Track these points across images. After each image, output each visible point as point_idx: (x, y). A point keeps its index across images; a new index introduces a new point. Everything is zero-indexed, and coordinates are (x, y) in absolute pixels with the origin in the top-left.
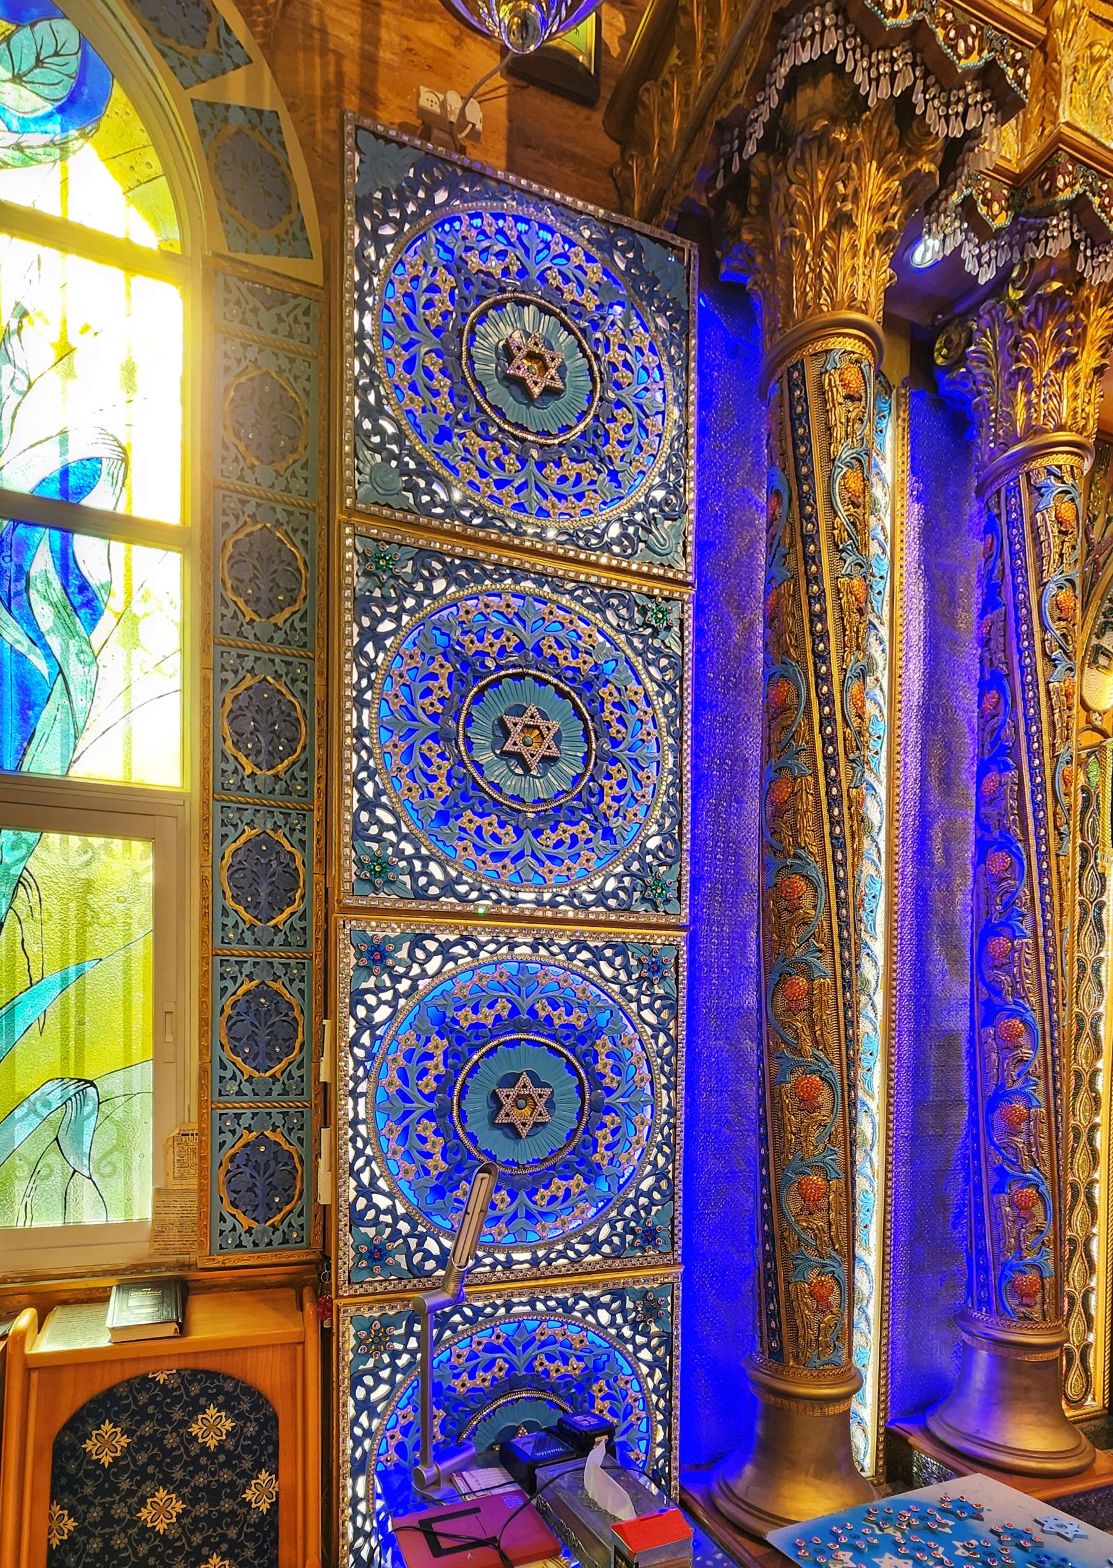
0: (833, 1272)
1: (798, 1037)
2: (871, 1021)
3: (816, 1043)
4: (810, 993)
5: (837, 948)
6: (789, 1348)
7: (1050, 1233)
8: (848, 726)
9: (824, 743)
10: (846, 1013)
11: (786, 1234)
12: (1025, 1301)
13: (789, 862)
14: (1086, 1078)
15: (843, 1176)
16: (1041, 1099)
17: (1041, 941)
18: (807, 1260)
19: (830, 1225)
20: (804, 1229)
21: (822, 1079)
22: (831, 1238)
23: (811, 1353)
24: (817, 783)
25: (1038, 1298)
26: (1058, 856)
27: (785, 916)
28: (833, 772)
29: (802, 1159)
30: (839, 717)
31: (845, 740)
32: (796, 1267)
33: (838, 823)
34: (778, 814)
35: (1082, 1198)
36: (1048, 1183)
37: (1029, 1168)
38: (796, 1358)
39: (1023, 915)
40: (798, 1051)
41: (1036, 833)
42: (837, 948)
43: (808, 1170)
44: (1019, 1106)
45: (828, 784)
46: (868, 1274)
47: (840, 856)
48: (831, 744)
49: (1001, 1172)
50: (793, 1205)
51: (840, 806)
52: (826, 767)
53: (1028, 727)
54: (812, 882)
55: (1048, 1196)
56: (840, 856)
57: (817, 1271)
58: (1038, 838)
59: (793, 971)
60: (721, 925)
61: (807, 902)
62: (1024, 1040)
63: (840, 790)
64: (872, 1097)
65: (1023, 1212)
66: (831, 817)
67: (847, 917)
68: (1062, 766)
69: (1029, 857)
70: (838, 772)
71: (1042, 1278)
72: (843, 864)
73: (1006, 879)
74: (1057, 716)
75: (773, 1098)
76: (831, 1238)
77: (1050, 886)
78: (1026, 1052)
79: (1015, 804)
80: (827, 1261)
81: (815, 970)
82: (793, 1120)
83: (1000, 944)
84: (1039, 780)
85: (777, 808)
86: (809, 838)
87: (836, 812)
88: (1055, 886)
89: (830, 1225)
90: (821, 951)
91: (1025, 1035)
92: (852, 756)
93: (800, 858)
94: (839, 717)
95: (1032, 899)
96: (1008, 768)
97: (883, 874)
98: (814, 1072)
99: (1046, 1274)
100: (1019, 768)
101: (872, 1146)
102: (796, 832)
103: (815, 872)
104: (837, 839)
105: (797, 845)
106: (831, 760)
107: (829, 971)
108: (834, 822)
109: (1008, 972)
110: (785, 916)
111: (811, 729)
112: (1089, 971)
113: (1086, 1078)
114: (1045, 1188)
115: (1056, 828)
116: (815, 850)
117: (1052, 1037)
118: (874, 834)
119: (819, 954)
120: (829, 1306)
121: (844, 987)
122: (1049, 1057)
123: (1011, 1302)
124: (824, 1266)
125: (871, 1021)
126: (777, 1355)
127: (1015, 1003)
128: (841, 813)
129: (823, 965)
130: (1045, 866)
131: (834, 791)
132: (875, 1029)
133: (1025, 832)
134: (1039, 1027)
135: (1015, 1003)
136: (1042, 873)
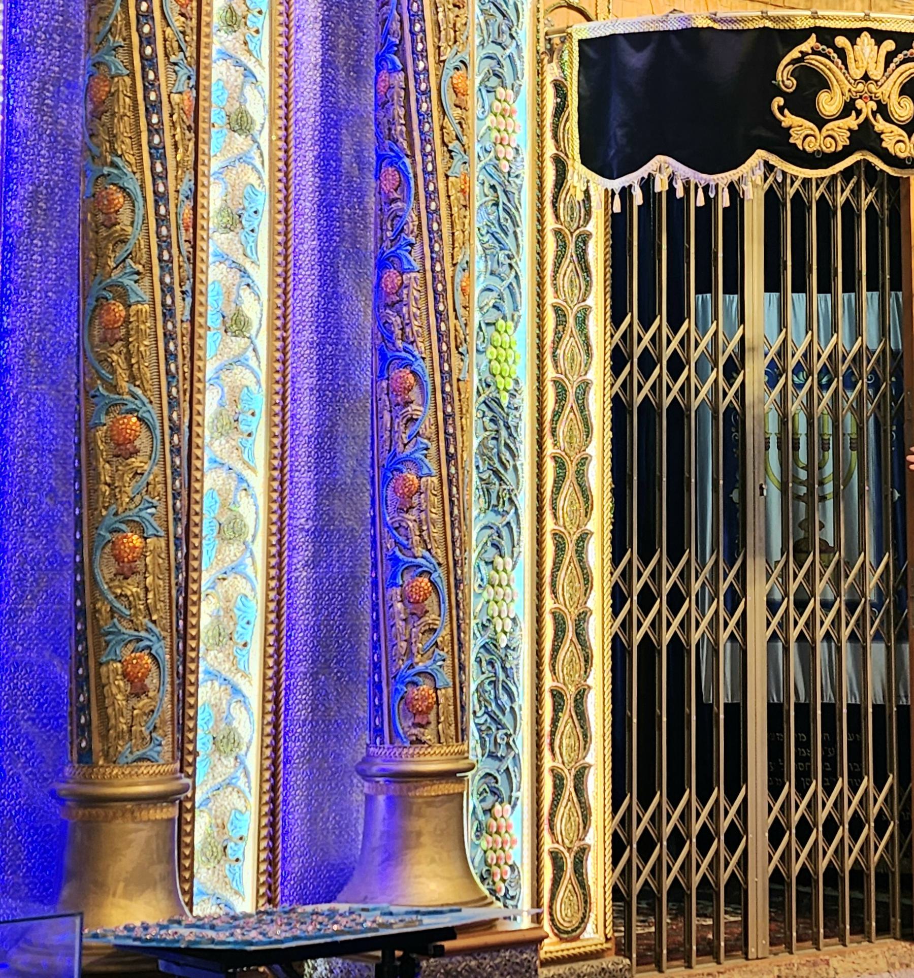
0: (149, 647)
1: (113, 372)
2: (253, 371)
3: (132, 379)
4: (127, 321)
5: (156, 271)
6: (97, 745)
7: (445, 632)
8: (168, 25)
9: (141, 42)
10: (166, 345)
11: (98, 605)
12: (418, 719)
13: (106, 170)
14: (571, 469)
15: (163, 533)
16: (433, 467)
17: (429, 275)
18: (119, 633)
19: (147, 590)
20: (117, 597)
21: (139, 419)
22: (147, 607)
23: (123, 747)
24: (134, 85)
25: (432, 717)
26: (447, 177)
27: (104, 232)
28: (151, 76)
29: (116, 514)
30: (157, 14)
31: (165, 40)
32: (107, 643)
33: (157, 131)
34: (97, 115)
35: (570, 634)
36: (441, 571)
37: (420, 551)
38: (106, 755)
39: (412, 245)
40: (113, 388)
41: (423, 149)
42: (156, 271)
43: (123, 527)
44: (411, 476)
45: (145, 88)
46: (248, 710)
47: (159, 168)
48: (149, 44)
49: (395, 560)
50: (105, 571)
51: (159, 113)
52: (143, 68)
53: (412, 24)
54: (129, 194)
55: (442, 586)
56: (159, 168)
57: (131, 647)
58: (424, 155)
59: (110, 295)
60: (45, 239)
61: (125, 217)
62: (415, 395)
63: (159, 96)
64: (254, 470)
65: (416, 611)
66: (149, 124)
67: (169, 236)
68: (449, 71)
69: (415, 176)
70: (157, 77)
71: (436, 689)
72: (164, 177)
73: (395, 200)
74: (441, 15)
75: (88, 444)
76: (147, 607)
77: (438, 210)
78: (414, 409)
79: (402, 112)
80: (143, 634)
81: (132, 295)
82: (106, 471)
83: (391, 278)
84: (423, 87)
85: (96, 108)
86: (124, 146)
87: (155, 120)
88: (444, 212)
89: (147, 590)
90: (138, 273)
91: (416, 389)
92: (173, 59)
93: (117, 167)
94: (157, 14)
95: (420, 227)
96: (395, 69)
97: (267, 184)
98: (131, 412)
99: (439, 684)
100: (405, 70)
101: (254, 536)
102: (113, 138)
103: (132, 185)
104: (157, 149)
105: (113, 152)
106: (149, 62)
107: (147, 297)
108: (153, 130)
109: (399, 313)
110: (104, 232)
111: (128, 25)
112: (571, 321)
113: (571, 469)
114: (439, 575)
115: (444, 144)
116: (132, 160)
117: (443, 392)
118: (255, 132)
119: (136, 277)
120: (144, 691)
121: (164, 314)
122: (440, 415)
123: (404, 725)
124: (140, 640)
125: (253, 371)
126: (86, 756)
127: (405, 350)
128: (161, 122)
129: (139, 291)
130: (431, 188)
131: (153, 96)
132: (258, 382)
133: (411, 146)
134: (427, 378)
135: (405, 350)
136: (429, 196)
